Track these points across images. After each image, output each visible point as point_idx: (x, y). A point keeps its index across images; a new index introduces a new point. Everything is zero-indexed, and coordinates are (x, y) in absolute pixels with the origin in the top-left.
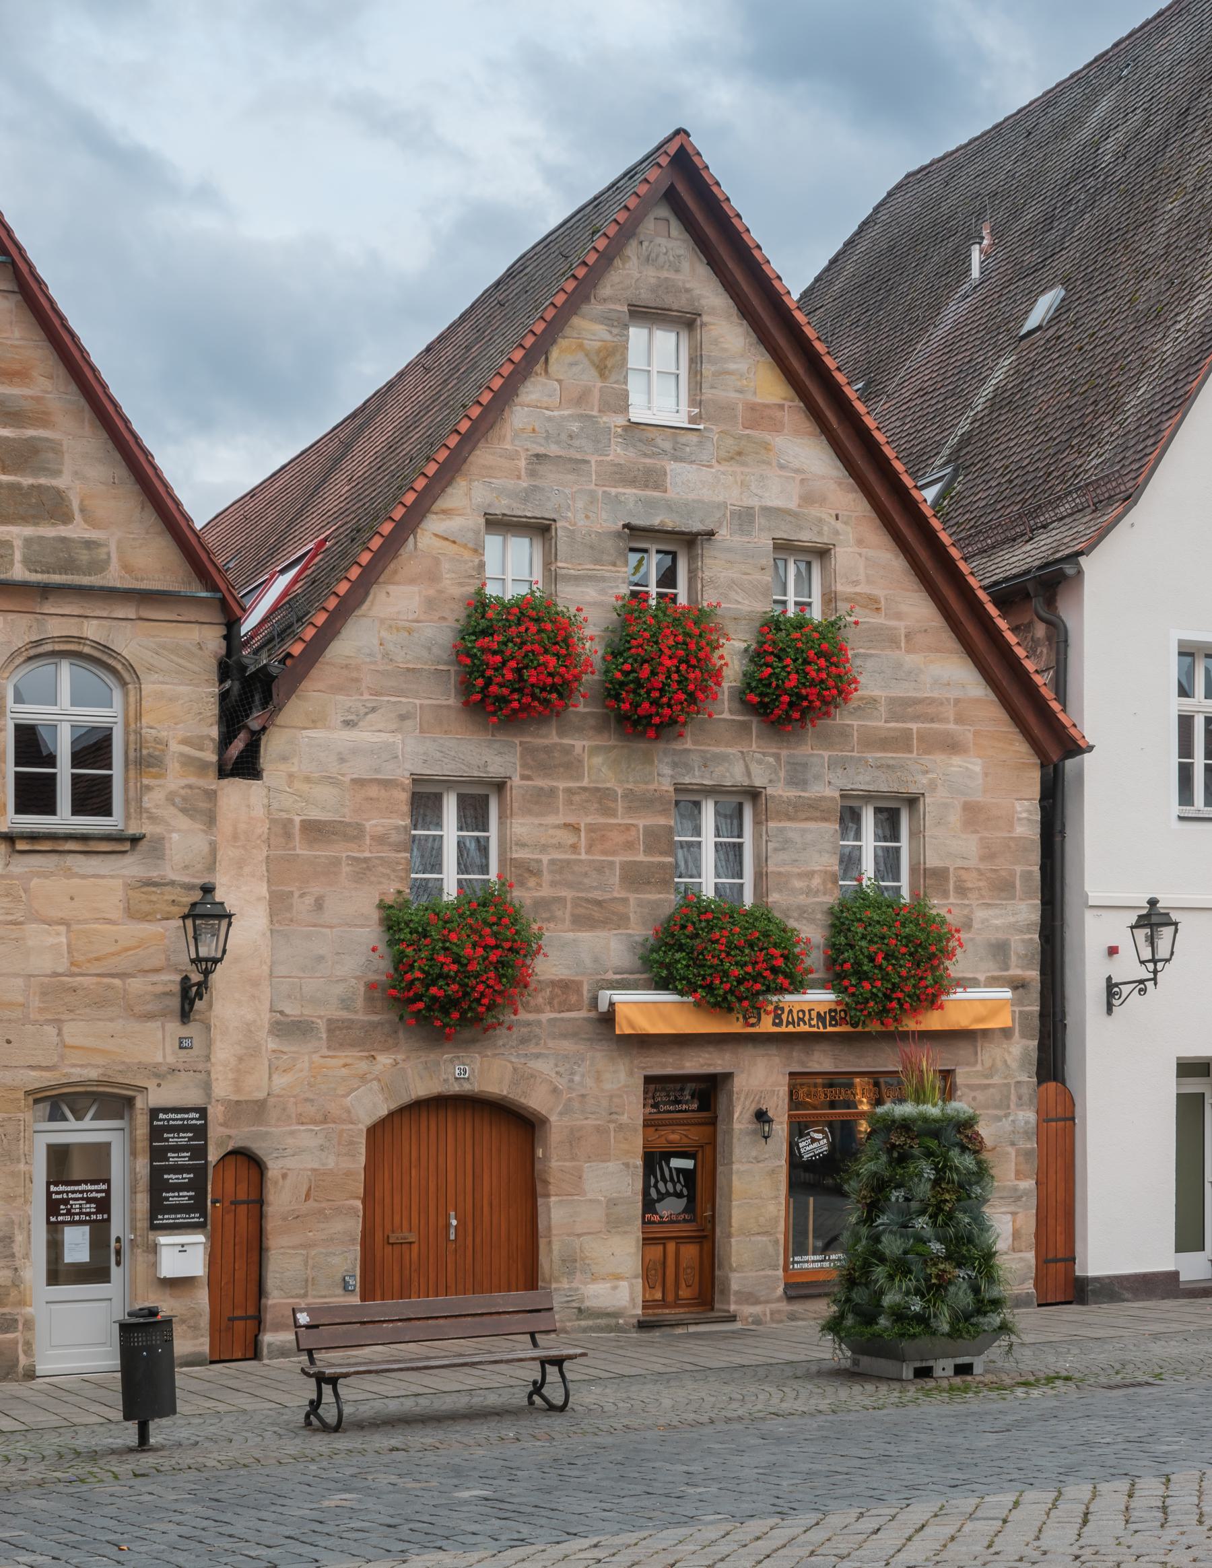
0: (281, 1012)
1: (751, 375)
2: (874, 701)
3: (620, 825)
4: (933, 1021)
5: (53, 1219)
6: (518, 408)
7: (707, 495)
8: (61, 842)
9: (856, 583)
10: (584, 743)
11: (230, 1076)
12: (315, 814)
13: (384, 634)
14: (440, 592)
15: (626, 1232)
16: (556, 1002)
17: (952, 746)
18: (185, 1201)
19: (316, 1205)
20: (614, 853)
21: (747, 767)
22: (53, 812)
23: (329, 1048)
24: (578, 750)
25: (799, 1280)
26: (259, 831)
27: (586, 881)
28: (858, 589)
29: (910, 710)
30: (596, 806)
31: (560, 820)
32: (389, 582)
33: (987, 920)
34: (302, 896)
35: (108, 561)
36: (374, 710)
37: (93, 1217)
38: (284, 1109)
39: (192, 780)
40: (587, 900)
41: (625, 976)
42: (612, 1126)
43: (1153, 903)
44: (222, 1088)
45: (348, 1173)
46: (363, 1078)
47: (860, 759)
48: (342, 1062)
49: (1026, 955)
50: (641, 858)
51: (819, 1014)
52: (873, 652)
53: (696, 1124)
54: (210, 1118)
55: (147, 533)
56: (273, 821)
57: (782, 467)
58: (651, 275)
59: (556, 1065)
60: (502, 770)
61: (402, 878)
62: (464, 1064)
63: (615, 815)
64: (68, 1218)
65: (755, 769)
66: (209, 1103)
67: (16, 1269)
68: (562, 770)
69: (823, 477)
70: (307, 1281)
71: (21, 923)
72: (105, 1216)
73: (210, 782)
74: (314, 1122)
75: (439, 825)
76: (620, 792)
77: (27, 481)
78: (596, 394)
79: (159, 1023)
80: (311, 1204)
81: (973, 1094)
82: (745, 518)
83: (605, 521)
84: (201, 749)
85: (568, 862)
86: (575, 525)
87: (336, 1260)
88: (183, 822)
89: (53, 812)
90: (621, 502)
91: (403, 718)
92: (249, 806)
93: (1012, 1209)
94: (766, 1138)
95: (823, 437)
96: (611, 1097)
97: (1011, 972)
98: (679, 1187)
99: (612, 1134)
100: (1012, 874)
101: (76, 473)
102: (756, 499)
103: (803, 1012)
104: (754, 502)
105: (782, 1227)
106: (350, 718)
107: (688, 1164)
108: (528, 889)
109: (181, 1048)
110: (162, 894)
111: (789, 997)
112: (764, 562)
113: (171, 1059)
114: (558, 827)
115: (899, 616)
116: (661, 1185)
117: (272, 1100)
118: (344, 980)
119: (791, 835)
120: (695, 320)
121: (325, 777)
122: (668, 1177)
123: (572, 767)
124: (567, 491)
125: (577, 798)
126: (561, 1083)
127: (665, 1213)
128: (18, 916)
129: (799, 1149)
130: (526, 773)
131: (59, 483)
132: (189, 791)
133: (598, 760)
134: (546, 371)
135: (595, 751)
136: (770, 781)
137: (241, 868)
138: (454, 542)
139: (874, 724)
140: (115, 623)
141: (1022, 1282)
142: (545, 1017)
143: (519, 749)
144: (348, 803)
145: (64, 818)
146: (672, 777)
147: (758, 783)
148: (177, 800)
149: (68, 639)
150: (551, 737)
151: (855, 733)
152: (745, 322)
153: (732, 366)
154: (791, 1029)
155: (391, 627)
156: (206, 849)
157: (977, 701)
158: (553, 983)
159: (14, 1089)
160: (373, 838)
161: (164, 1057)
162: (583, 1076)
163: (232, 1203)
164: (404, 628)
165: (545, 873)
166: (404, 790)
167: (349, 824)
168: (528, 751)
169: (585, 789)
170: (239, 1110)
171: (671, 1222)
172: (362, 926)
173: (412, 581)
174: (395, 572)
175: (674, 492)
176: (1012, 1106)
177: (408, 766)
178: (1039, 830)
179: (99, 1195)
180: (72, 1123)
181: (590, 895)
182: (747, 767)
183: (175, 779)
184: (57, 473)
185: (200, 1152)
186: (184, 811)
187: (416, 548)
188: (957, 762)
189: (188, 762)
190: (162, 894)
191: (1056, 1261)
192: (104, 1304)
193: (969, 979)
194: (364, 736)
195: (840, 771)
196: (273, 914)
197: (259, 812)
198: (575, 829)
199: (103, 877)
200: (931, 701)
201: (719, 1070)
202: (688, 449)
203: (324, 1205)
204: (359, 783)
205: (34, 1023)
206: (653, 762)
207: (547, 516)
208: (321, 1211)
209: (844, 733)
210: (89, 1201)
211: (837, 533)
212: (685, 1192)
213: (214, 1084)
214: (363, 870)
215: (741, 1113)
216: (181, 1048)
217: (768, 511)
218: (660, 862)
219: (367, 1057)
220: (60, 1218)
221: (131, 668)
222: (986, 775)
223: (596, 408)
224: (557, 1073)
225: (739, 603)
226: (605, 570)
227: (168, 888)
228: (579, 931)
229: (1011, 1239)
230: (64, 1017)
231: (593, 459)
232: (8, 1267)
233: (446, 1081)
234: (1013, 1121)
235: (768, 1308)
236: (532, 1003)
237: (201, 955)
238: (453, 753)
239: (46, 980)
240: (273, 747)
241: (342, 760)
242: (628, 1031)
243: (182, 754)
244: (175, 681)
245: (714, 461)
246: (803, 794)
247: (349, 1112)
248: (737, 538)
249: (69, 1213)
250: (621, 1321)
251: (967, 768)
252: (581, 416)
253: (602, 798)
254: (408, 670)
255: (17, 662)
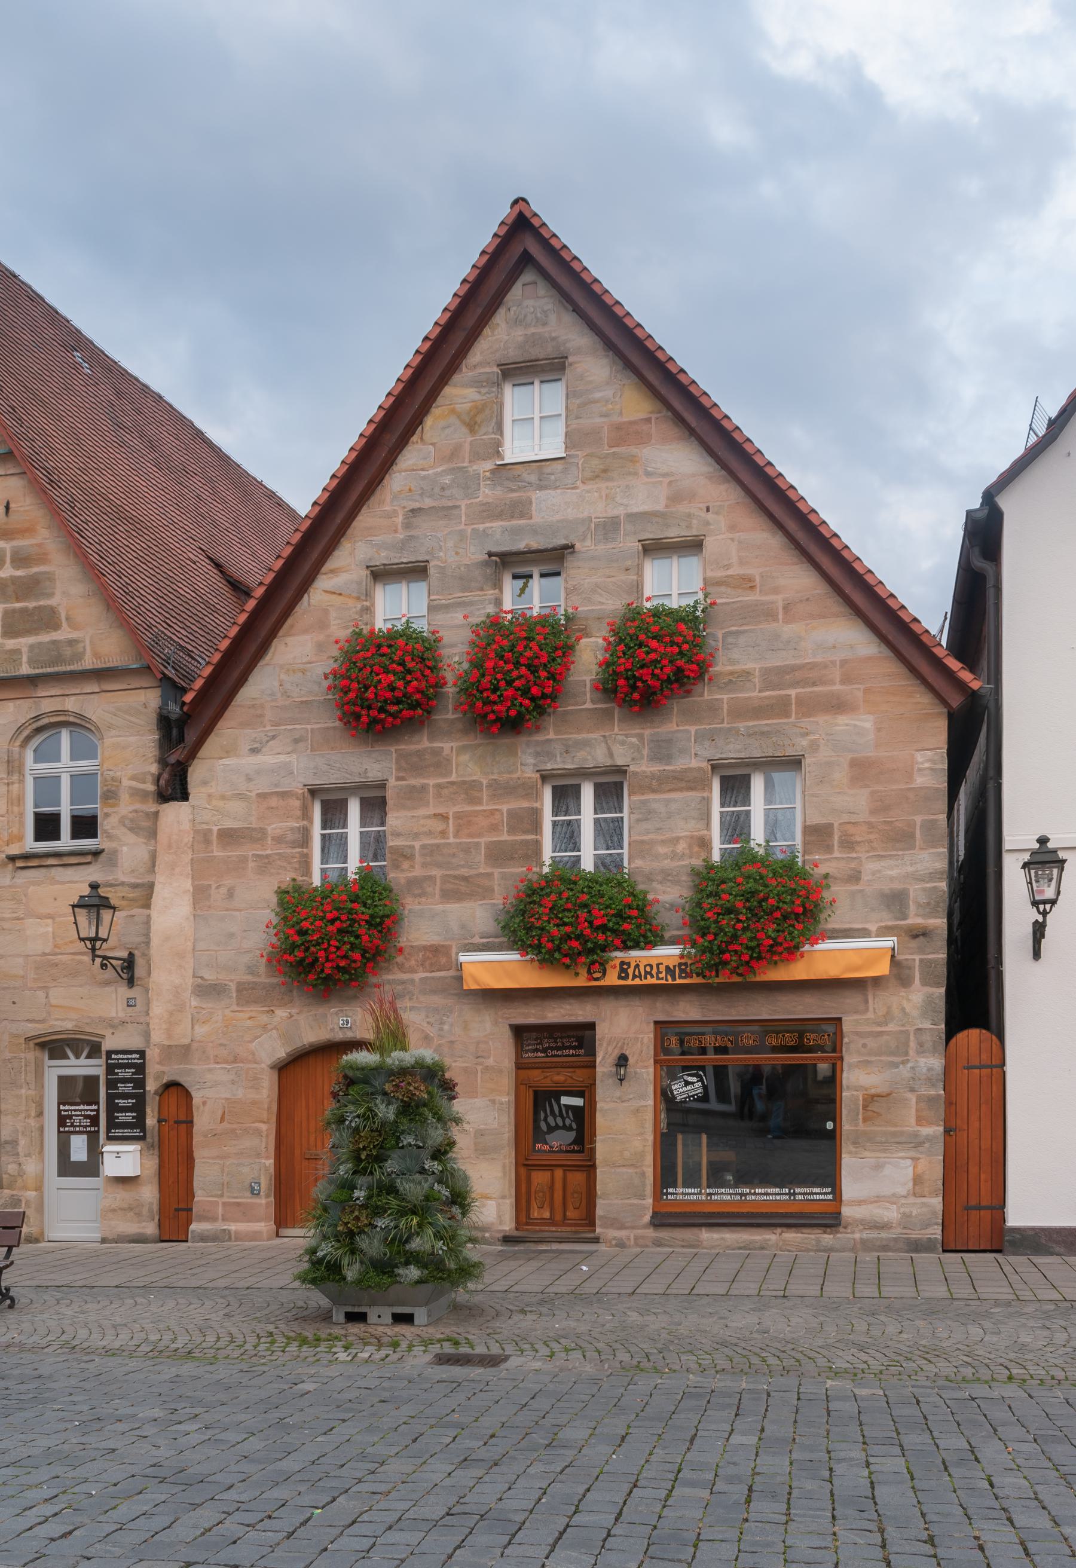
0: (202, 978)
1: (617, 399)
2: (747, 674)
3: (485, 811)
4: (798, 971)
5: (62, 1129)
6: (397, 474)
7: (571, 514)
8: (44, 859)
9: (728, 567)
10: (452, 744)
11: (164, 1026)
12: (229, 824)
13: (283, 676)
14: (329, 636)
15: (493, 1159)
16: (427, 963)
17: (838, 706)
18: (130, 1120)
19: (229, 1126)
20: (480, 835)
21: (609, 749)
22: (58, 838)
23: (238, 1004)
24: (447, 751)
25: (688, 1210)
26: (186, 840)
27: (454, 860)
28: (730, 572)
29: (788, 677)
30: (463, 796)
31: (431, 811)
32: (288, 635)
33: (879, 871)
34: (217, 888)
35: (84, 652)
36: (274, 737)
37: (88, 1129)
38: (204, 1052)
39: (138, 806)
40: (455, 877)
41: (491, 940)
42: (479, 1068)
43: (1043, 841)
44: (158, 1036)
45: (254, 1103)
46: (264, 1028)
47: (730, 729)
48: (247, 1015)
49: (928, 904)
50: (505, 837)
51: (667, 968)
52: (746, 628)
53: (583, 1067)
54: (147, 1058)
55: (110, 627)
56: (196, 832)
57: (648, 474)
58: (519, 334)
59: (427, 1017)
60: (380, 774)
61: (296, 869)
62: (347, 1016)
63: (480, 803)
64: (72, 1129)
65: (617, 749)
66: (148, 1047)
67: (20, 1164)
68: (432, 769)
69: (693, 475)
70: (223, 1184)
71: (22, 919)
72: (96, 1129)
73: (152, 807)
74: (227, 1062)
75: (345, 826)
76: (485, 782)
77: (31, 605)
78: (467, 447)
79: (113, 988)
80: (226, 1125)
81: (862, 1041)
82: (610, 527)
83: (473, 554)
84: (144, 783)
85: (438, 846)
86: (446, 562)
87: (245, 1170)
88: (131, 838)
89: (58, 838)
90: (488, 535)
91: (296, 741)
92: (178, 822)
93: (912, 1154)
94: (621, 1080)
95: (693, 438)
96: (478, 1043)
97: (909, 921)
98: (568, 1122)
99: (479, 1074)
100: (911, 824)
101: (64, 593)
102: (622, 508)
103: (651, 966)
104: (620, 511)
105: (649, 1159)
106: (255, 746)
107: (578, 1102)
108: (403, 871)
109: (128, 1006)
110: (115, 892)
111: (635, 953)
112: (629, 563)
113: (121, 1015)
114: (428, 817)
115: (776, 590)
116: (551, 1120)
117: (195, 1045)
118: (249, 951)
119: (654, 806)
120: (565, 362)
121: (234, 794)
122: (557, 1112)
123: (441, 765)
124: (439, 535)
125: (445, 792)
126: (432, 1032)
127: (555, 1144)
128: (20, 914)
129: (671, 1091)
130: (401, 774)
131: (52, 602)
132: (135, 815)
133: (465, 758)
134: (422, 439)
135: (463, 749)
136: (633, 759)
137: (173, 869)
138: (340, 594)
139: (747, 695)
140: (86, 697)
141: (927, 1226)
142: (417, 976)
143: (394, 755)
144: (254, 813)
145: (66, 841)
146: (535, 765)
147: (620, 762)
148: (127, 822)
149: (57, 713)
150: (423, 742)
151: (725, 706)
152: (611, 352)
153: (598, 395)
154: (637, 981)
155: (288, 670)
156: (146, 856)
157: (869, 659)
158: (425, 948)
159: (17, 1036)
160: (273, 839)
161: (117, 1013)
162: (452, 1025)
163: (176, 1122)
164: (299, 670)
165: (417, 855)
166: (297, 798)
167: (254, 829)
168: (402, 756)
169: (452, 783)
170: (171, 1052)
171: (560, 1151)
172: (263, 908)
173: (305, 631)
174: (292, 626)
175: (539, 516)
176: (911, 1053)
177: (303, 780)
178: (946, 779)
179: (92, 1113)
180: (73, 1060)
181: (457, 873)
182: (609, 749)
183: (126, 806)
184: (51, 595)
185: (140, 1084)
186: (131, 829)
187: (309, 605)
188: (843, 722)
189: (136, 793)
190: (115, 892)
191: (979, 1208)
192: (96, 1192)
193: (858, 930)
194: (266, 759)
195: (707, 743)
196: (195, 903)
197: (186, 826)
198: (444, 817)
199: (76, 882)
200: (812, 666)
201: (580, 1019)
202: (553, 477)
203: (234, 1126)
204: (262, 796)
205: (31, 989)
206: (517, 754)
207: (421, 559)
208: (233, 1131)
209: (713, 708)
210: (86, 1117)
211: (708, 523)
212: (574, 1126)
213: (152, 1033)
214: (265, 864)
215: (603, 1058)
216: (128, 1006)
217: (632, 517)
218: (523, 840)
219: (268, 1012)
220: (67, 1129)
221: (97, 728)
222: (879, 730)
223: (467, 460)
224: (428, 1023)
225: (603, 603)
226: (474, 596)
227: (120, 888)
228: (448, 903)
229: (910, 1185)
230: (49, 985)
231: (463, 504)
232: (15, 1162)
233: (332, 1030)
234: (913, 1068)
235: (633, 1234)
236: (407, 965)
237: (100, 935)
238: (338, 765)
239: (38, 958)
240: (196, 774)
241: (249, 779)
242: (474, 987)
243: (130, 787)
244: (127, 734)
245: (578, 483)
246: (667, 768)
247: (254, 1054)
248: (601, 547)
249: (72, 1125)
250: (487, 1235)
251: (855, 726)
252: (453, 469)
253: (469, 790)
254: (302, 702)
255: (26, 733)
